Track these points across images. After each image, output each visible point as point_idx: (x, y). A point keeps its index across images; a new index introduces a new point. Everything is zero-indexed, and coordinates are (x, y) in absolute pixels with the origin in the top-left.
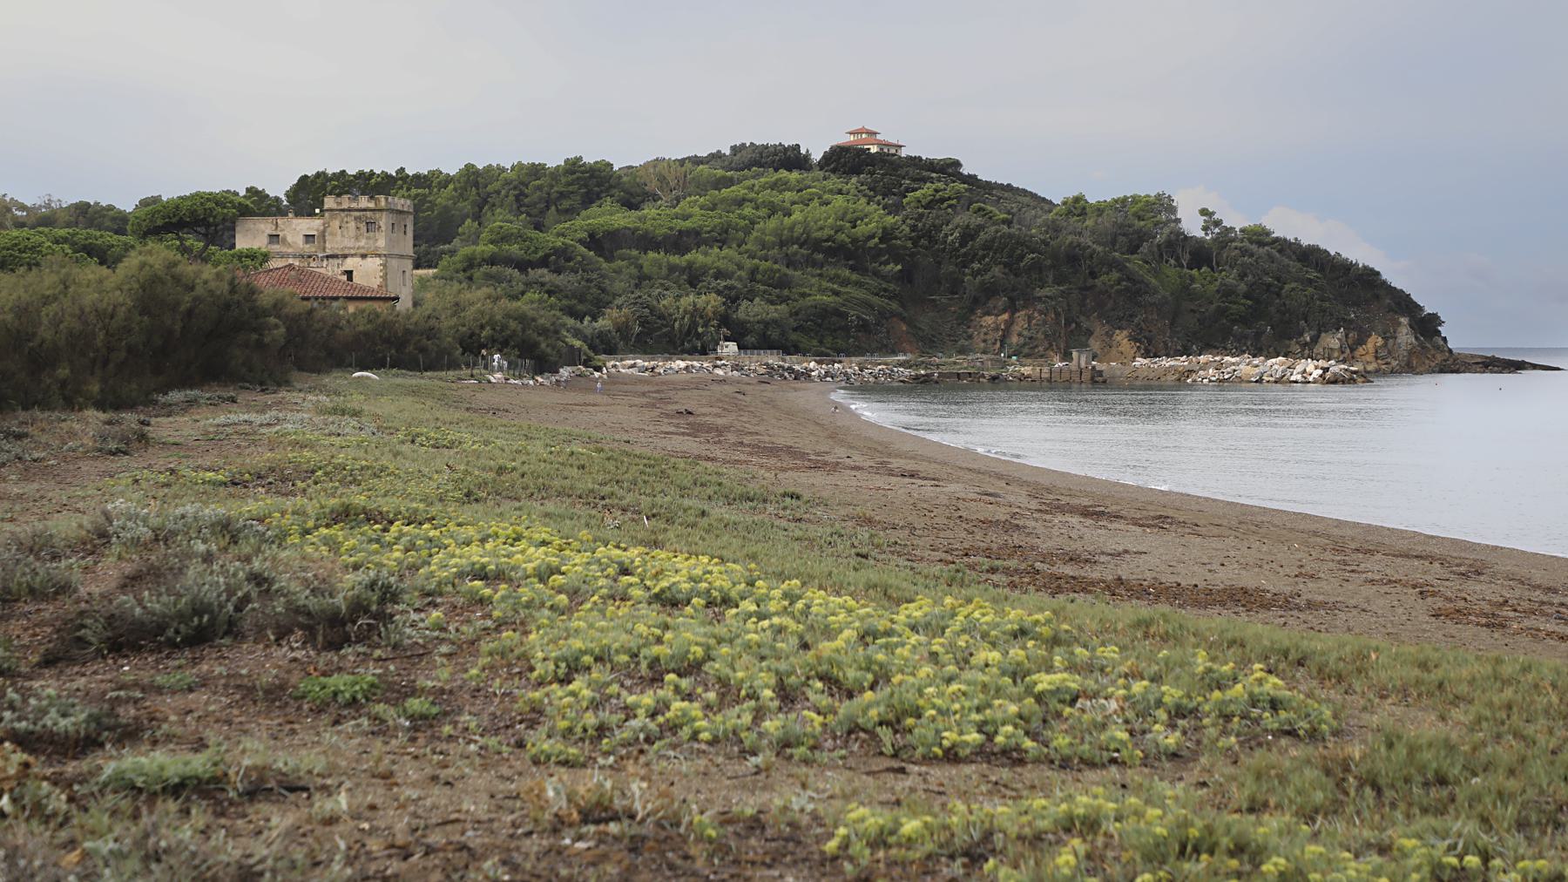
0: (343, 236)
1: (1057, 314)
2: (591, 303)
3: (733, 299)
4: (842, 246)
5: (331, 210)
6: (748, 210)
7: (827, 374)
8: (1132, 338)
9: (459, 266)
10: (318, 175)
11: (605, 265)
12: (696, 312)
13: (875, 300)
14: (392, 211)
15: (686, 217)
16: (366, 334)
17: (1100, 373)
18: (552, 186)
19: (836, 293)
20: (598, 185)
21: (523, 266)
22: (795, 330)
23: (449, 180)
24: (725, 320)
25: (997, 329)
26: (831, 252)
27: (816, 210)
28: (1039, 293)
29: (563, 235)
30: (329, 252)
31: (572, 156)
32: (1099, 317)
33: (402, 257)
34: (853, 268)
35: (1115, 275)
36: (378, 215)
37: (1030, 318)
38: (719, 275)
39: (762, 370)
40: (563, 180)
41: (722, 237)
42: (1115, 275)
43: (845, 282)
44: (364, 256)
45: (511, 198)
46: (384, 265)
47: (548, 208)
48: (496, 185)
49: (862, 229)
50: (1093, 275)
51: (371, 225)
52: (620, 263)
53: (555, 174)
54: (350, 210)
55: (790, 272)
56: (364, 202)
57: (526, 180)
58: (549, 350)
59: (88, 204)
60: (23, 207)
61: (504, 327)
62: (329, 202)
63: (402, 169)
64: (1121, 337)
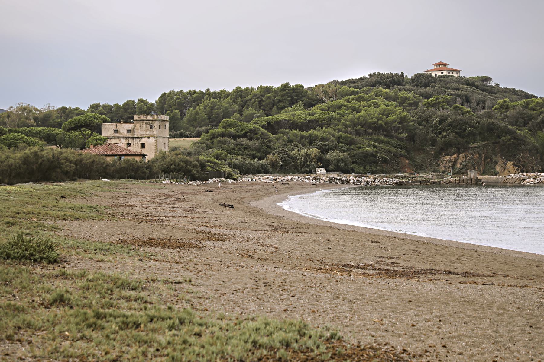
1: (480, 155)
3: (324, 150)
4: (381, 126)
5: (136, 120)
6: (342, 111)
8: (515, 165)
9: (208, 137)
10: (170, 93)
11: (272, 136)
13: (394, 150)
14: (159, 120)
15: (313, 114)
16: (125, 168)
17: (480, 180)
18: (275, 97)
19: (375, 147)
20: (297, 96)
21: (235, 137)
22: (353, 163)
23: (229, 94)
24: (320, 159)
25: (450, 162)
26: (375, 129)
27: (372, 110)
28: (472, 145)
30: (136, 136)
32: (501, 156)
33: (163, 137)
34: (385, 136)
35: (508, 137)
36: (154, 122)
37: (466, 157)
38: (323, 139)
39: (326, 180)
40: (280, 94)
41: (328, 123)
42: (508, 137)
43: (381, 142)
44: (149, 138)
45: (257, 103)
46: (156, 141)
47: (273, 106)
48: (250, 97)
50: (499, 137)
52: (280, 135)
53: (276, 92)
54: (143, 120)
55: (358, 138)
59: (66, 108)
62: (136, 117)
63: (208, 90)
64: (510, 164)
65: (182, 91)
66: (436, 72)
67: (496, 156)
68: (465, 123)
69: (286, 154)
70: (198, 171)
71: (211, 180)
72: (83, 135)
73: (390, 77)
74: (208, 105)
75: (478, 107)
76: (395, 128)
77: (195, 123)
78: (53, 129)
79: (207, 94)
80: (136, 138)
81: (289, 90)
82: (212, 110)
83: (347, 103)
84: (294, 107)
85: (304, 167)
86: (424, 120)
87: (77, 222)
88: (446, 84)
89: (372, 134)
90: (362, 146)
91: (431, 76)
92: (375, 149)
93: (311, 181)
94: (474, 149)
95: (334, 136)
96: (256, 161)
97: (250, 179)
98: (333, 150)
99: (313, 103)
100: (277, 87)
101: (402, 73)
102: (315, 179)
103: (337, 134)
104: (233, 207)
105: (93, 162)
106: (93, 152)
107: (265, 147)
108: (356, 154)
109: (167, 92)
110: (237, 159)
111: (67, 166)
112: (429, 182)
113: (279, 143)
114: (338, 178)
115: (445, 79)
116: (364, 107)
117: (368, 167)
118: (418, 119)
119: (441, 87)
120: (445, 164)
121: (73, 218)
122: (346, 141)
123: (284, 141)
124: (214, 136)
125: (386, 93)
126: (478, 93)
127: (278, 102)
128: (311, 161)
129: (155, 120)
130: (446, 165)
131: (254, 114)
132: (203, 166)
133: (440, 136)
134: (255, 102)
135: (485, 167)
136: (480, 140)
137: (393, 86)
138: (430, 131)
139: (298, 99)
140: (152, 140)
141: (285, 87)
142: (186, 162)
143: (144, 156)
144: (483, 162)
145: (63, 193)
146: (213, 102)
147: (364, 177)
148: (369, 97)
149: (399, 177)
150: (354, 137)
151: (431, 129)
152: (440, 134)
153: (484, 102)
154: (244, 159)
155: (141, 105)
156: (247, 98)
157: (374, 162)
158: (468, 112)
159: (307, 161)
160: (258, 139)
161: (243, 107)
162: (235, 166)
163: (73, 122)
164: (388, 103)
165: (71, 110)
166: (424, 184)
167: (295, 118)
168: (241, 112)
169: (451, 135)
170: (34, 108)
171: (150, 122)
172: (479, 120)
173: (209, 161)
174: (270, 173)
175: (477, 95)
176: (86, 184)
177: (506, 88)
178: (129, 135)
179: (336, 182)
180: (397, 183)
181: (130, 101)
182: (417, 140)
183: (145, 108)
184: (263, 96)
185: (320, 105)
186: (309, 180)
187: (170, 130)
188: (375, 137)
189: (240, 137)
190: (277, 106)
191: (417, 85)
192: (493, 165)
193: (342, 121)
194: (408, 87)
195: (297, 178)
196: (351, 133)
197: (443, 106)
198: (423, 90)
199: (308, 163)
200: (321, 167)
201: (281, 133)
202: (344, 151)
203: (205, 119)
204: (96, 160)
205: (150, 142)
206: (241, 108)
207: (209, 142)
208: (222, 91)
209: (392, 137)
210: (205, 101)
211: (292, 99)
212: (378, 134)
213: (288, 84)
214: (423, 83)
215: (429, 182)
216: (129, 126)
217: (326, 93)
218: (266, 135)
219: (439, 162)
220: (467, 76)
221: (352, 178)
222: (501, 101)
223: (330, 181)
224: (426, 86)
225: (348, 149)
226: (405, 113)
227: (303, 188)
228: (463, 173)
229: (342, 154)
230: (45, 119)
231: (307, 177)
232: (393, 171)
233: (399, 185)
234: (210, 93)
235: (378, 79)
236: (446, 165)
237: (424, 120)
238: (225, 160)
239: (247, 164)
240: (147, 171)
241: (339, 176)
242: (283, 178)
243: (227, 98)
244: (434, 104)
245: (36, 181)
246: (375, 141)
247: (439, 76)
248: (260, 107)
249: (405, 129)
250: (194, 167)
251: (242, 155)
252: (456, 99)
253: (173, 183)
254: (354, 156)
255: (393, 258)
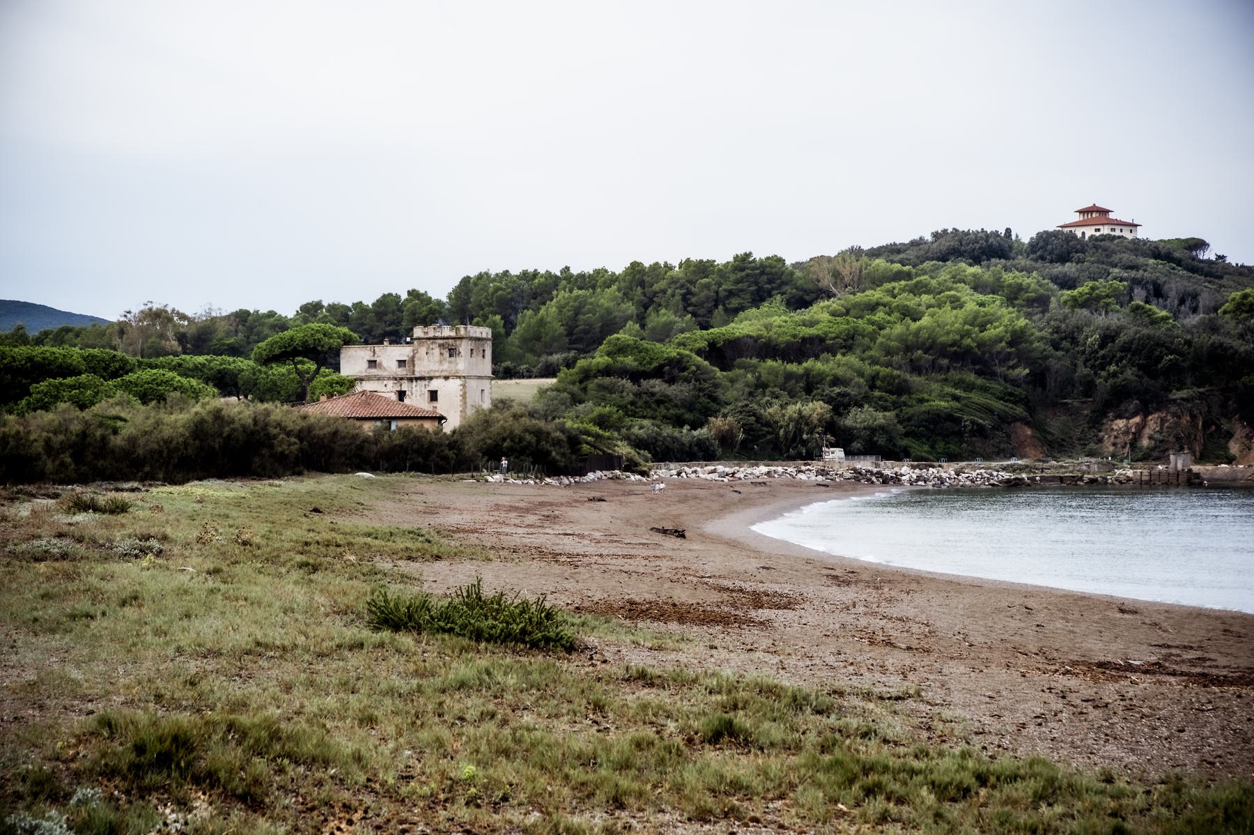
0: (429, 361)
1: (1193, 417)
2: (699, 411)
3: (840, 406)
4: (968, 350)
5: (419, 339)
6: (880, 315)
7: (919, 478)
9: (574, 378)
10: (480, 276)
11: (719, 374)
12: (801, 419)
13: (998, 405)
14: (471, 339)
15: (812, 324)
16: (401, 446)
17: (1198, 475)
18: (720, 285)
19: (956, 398)
21: (635, 376)
22: (907, 435)
23: (614, 279)
25: (1127, 432)
29: (684, 345)
30: (417, 375)
31: (741, 252)
33: (480, 377)
34: (979, 373)
36: (458, 342)
37: (1163, 421)
38: (836, 381)
39: (848, 475)
40: (733, 277)
41: (848, 343)
43: (969, 387)
44: (446, 378)
45: (678, 297)
46: (464, 386)
47: (716, 306)
49: (992, 332)
51: (453, 352)
52: (738, 371)
53: (723, 272)
54: (435, 338)
56: (447, 331)
57: (692, 277)
58: (558, 457)
59: (247, 313)
60: (183, 317)
61: (521, 439)
63: (567, 268)
65: (506, 273)
66: (1083, 229)
67: (1230, 419)
68: (1158, 344)
69: (754, 415)
70: (563, 455)
71: (591, 476)
72: (299, 373)
73: (981, 238)
74: (567, 304)
75: (1183, 308)
76: (1001, 356)
77: (538, 346)
78: (231, 359)
79: (565, 279)
80: (417, 379)
81: (753, 269)
82: (576, 314)
83: (889, 299)
84: (765, 307)
85: (792, 445)
86: (1065, 338)
87: (438, 565)
88: (1107, 256)
89: (948, 368)
90: (926, 396)
91: (1074, 237)
92: (955, 404)
93: (813, 478)
94: (1179, 405)
95: (861, 374)
96: (685, 431)
97: (674, 472)
98: (861, 406)
99: (807, 298)
100: (724, 262)
101: (1008, 231)
102: (819, 473)
103: (869, 369)
104: (683, 536)
105: (336, 433)
106: (326, 410)
107: (704, 400)
108: (913, 415)
109: (473, 274)
110: (643, 427)
111: (282, 442)
112: (1081, 479)
113: (737, 389)
114: (875, 470)
115: (1107, 243)
116: (929, 306)
117: (940, 446)
118: (1052, 334)
119: (1098, 262)
120: (1116, 437)
121: (428, 556)
122: (889, 384)
123: (747, 385)
124: (586, 375)
125: (974, 275)
126: (1181, 277)
127: (727, 297)
128: (811, 432)
129: (461, 338)
130: (1118, 441)
131: (672, 323)
132: (573, 441)
133: (1103, 373)
134: (673, 296)
135: (1205, 445)
136: (1193, 384)
137: (988, 259)
138: (1080, 363)
139: (773, 289)
140: (455, 384)
141: (743, 262)
142: (538, 433)
143: (441, 419)
144: (1200, 435)
145: (318, 502)
146: (578, 297)
147: (933, 467)
148: (939, 284)
149: (1013, 469)
150: (908, 376)
151: (1082, 358)
152: (1103, 369)
153: (1195, 296)
154: (658, 427)
155: (414, 306)
156: (656, 287)
157: (954, 433)
158: (1165, 319)
159: (801, 432)
160: (689, 382)
161: (646, 307)
162: (638, 444)
163: (276, 342)
164: (982, 297)
165: (259, 317)
166: (1071, 486)
167: (771, 333)
168: (641, 319)
169: (1129, 372)
170: (178, 313)
171: (450, 341)
172: (1189, 337)
173: (588, 433)
174: (718, 460)
175: (1177, 283)
176: (329, 484)
177: (1242, 266)
178: (401, 372)
179: (869, 480)
180: (1008, 481)
181: (390, 295)
182: (1051, 383)
183: (424, 310)
184: (692, 282)
185: (826, 303)
186: (808, 474)
187: (495, 360)
188: (955, 375)
189: (648, 375)
190: (724, 305)
191: (1042, 258)
192: (1222, 441)
193: (880, 340)
194: (1022, 261)
195: (780, 469)
196: (899, 368)
197: (1108, 304)
198: (1058, 269)
199: (805, 436)
200: (833, 445)
201: (740, 367)
202: (885, 409)
203: (560, 335)
204: (341, 428)
205: (449, 391)
206: (642, 309)
207: (576, 388)
208: (597, 272)
209: (992, 375)
210: (561, 295)
211: (759, 290)
212: (961, 369)
213: (750, 254)
214: (1056, 252)
215: (1081, 479)
216: (403, 352)
217: (836, 275)
218: (706, 372)
219: (1101, 434)
220: (1154, 237)
221: (906, 470)
222: (1237, 295)
223: (855, 478)
224: (1063, 258)
225: (894, 403)
226: (1022, 322)
227: (800, 494)
228: (1157, 459)
229: (881, 415)
230: (200, 337)
231: (803, 468)
232: (998, 454)
233: (1013, 486)
234: (572, 276)
235: (955, 243)
236: (1118, 441)
237: (1066, 338)
238: (618, 430)
239: (665, 438)
240: (451, 454)
241: (877, 466)
242: (749, 470)
243: (609, 287)
244: (1088, 300)
245: (221, 475)
246: (956, 385)
247: (1091, 237)
248: (685, 308)
249: (1024, 358)
250: (554, 445)
251: (654, 418)
252: (1131, 290)
253: (511, 481)
254: (909, 419)
255: (1191, 648)
